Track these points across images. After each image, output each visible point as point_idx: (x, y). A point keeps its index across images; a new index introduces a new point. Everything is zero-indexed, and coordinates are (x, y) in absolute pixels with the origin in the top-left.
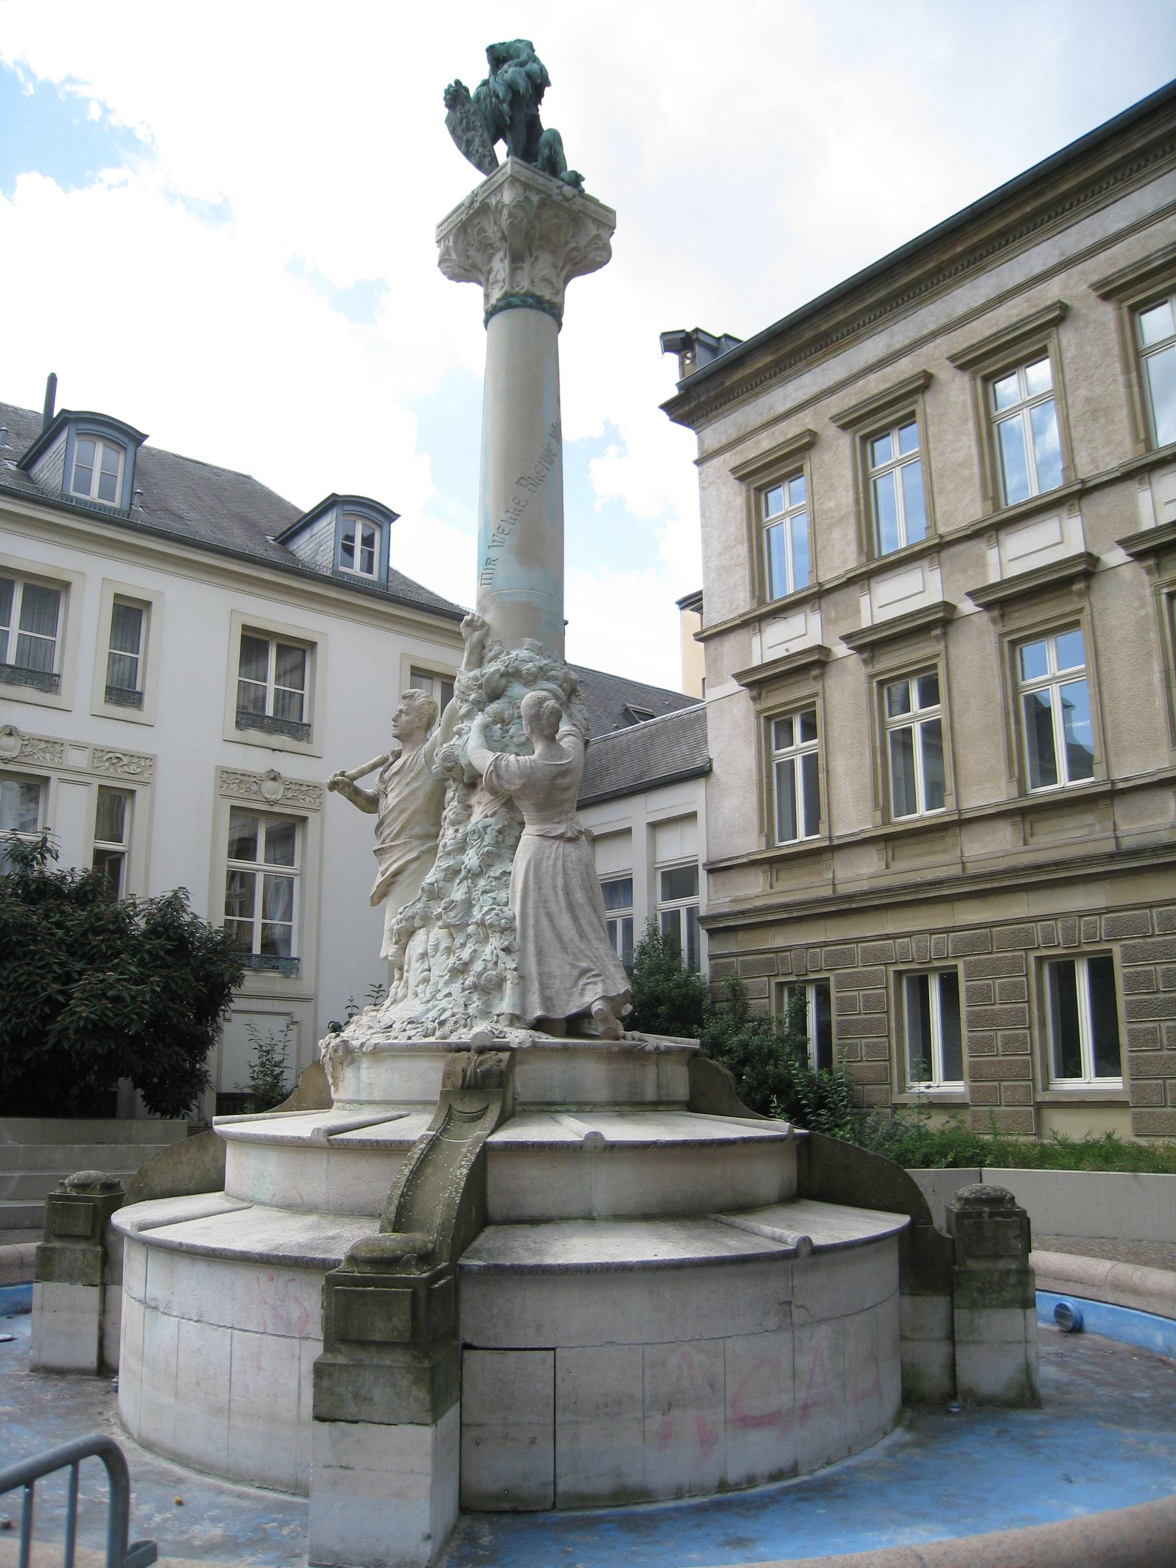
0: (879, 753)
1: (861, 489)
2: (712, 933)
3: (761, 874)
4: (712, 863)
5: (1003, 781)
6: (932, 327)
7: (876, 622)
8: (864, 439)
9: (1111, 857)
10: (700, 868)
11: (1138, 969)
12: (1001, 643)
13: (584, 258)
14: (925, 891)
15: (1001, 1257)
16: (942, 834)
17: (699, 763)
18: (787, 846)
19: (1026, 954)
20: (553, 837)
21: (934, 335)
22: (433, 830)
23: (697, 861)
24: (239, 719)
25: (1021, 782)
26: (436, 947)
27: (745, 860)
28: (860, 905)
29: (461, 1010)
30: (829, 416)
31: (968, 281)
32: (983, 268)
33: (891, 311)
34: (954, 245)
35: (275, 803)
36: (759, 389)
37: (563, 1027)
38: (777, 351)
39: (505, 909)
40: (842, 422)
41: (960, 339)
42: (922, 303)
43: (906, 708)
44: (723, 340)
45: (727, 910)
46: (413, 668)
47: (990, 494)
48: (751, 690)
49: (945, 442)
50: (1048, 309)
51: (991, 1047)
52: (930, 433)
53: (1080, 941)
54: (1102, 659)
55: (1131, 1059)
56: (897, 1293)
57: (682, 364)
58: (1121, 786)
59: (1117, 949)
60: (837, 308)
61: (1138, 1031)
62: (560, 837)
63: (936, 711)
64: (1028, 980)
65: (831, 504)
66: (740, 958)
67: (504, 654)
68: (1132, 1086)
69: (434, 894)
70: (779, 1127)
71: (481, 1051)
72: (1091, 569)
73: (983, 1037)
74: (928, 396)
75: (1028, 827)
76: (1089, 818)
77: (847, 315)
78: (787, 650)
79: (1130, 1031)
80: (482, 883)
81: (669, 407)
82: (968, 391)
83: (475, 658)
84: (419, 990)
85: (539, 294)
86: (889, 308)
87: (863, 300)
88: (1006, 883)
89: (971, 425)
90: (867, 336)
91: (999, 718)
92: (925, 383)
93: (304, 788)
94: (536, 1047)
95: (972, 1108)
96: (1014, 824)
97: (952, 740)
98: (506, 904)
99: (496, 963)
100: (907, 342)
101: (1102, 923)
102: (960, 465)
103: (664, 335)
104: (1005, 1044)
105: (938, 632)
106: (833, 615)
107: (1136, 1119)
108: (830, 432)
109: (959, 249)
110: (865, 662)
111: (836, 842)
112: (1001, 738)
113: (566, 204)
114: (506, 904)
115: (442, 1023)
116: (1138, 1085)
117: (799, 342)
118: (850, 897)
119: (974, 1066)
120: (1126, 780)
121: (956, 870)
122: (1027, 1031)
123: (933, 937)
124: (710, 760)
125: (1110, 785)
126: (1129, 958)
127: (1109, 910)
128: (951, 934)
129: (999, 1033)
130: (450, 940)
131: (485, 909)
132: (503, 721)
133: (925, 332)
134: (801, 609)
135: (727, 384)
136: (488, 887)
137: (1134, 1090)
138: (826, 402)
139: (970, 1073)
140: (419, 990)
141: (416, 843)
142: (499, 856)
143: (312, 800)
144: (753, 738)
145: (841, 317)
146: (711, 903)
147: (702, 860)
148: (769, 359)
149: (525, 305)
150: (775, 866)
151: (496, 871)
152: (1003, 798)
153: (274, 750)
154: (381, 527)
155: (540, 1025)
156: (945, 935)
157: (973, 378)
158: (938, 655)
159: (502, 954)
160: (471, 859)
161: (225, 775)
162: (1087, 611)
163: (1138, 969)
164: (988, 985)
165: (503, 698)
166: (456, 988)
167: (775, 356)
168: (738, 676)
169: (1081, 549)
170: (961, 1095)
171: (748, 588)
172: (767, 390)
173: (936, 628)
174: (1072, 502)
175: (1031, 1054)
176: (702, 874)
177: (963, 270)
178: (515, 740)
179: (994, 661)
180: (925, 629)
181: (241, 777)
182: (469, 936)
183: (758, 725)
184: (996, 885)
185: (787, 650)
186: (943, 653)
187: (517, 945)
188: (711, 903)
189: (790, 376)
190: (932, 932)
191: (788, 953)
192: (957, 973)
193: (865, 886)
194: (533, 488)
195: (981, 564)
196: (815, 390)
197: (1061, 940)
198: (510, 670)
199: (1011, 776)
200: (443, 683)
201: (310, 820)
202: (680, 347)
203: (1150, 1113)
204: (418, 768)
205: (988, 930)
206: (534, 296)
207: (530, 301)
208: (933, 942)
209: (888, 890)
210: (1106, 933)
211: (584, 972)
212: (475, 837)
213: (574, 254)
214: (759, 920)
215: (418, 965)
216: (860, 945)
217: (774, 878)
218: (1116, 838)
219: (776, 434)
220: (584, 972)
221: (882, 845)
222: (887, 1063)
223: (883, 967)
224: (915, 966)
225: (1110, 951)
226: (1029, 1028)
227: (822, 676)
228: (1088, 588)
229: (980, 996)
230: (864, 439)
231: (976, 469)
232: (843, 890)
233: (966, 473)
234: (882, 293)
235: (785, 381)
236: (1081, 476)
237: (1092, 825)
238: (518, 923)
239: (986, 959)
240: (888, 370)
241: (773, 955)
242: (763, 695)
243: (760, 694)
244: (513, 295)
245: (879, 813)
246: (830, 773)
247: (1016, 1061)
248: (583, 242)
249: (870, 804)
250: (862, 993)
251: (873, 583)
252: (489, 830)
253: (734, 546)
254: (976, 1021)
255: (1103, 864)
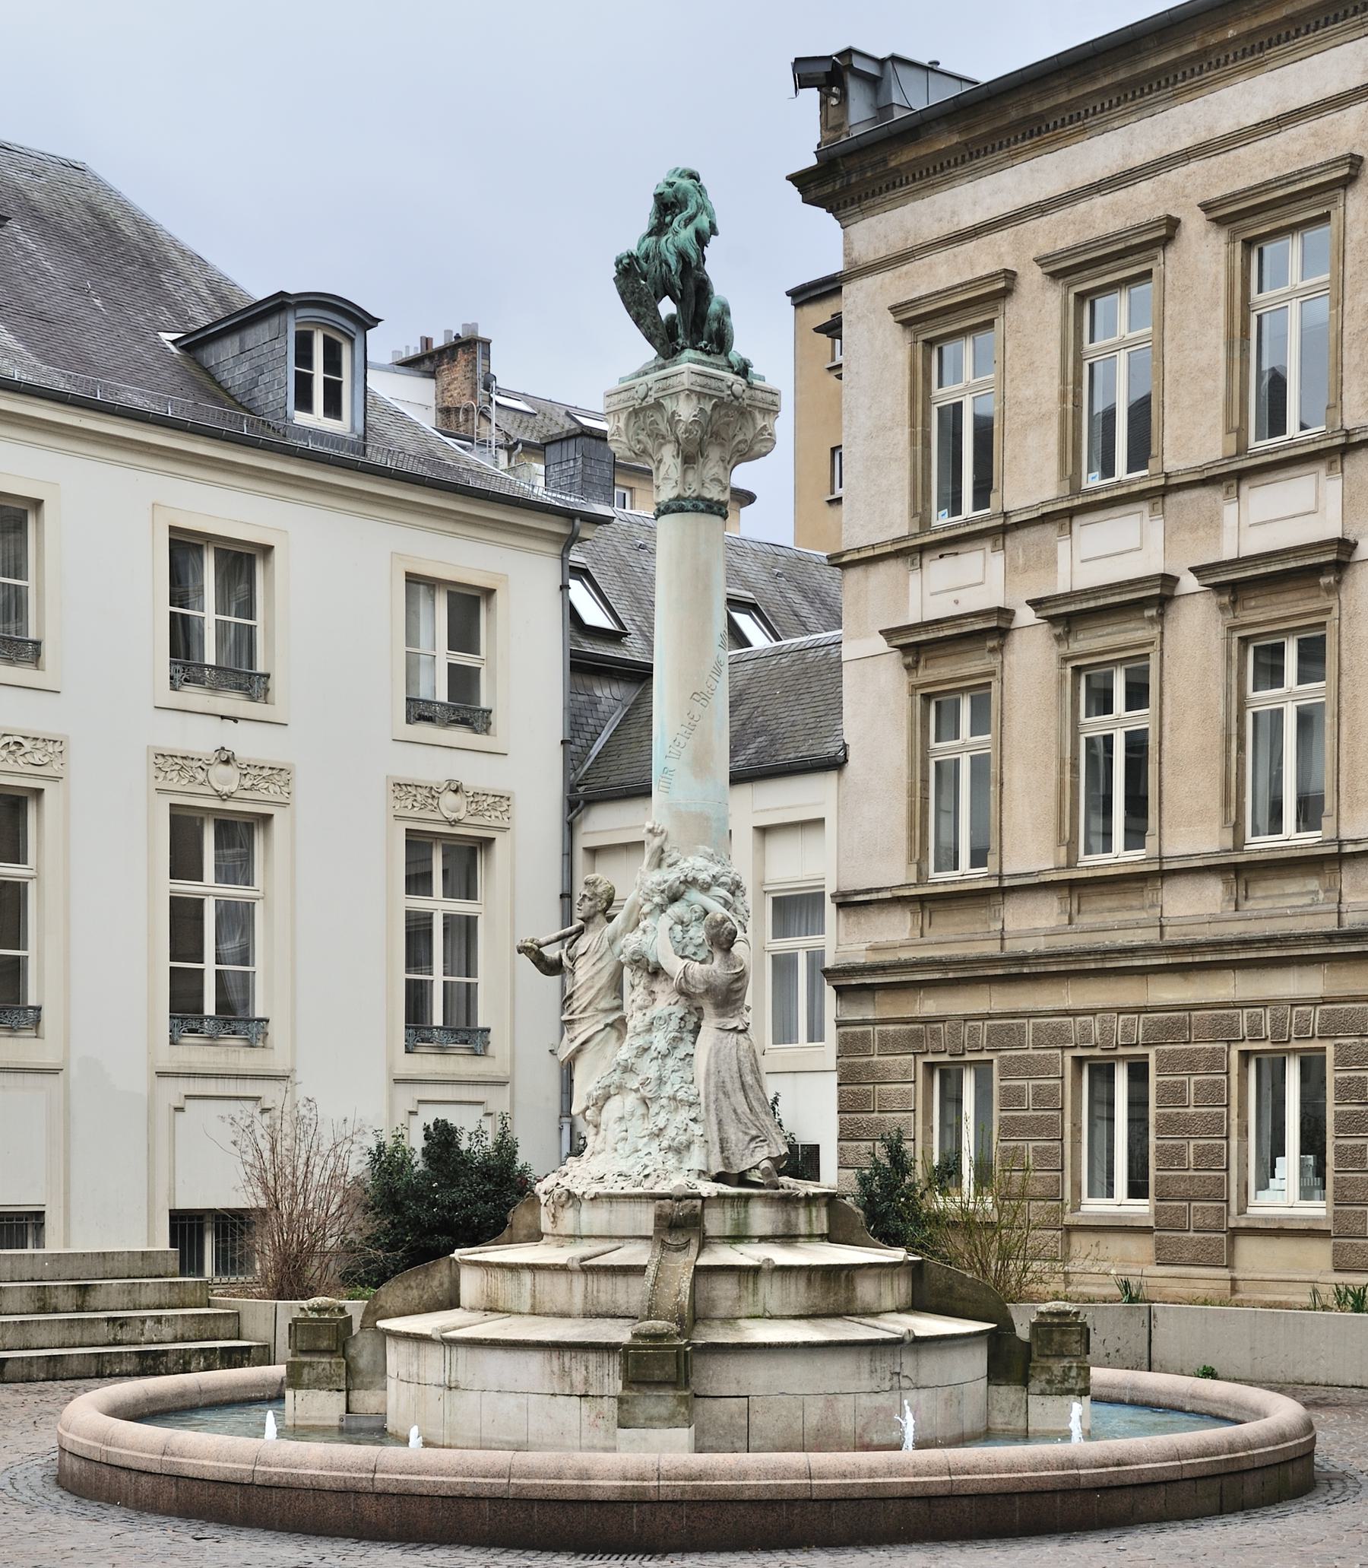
0: (1068, 768)
1: (1070, 378)
2: (840, 991)
3: (909, 915)
4: (844, 894)
5: (1217, 826)
6: (1187, 142)
7: (1074, 589)
8: (1081, 297)
9: (1330, 937)
10: (828, 899)
11: (1352, 1074)
12: (1228, 638)
13: (751, 448)
14: (1111, 959)
15: (1066, 1356)
16: (1139, 885)
17: (832, 748)
18: (941, 880)
19: (1229, 1047)
20: (729, 1030)
21: (1186, 156)
22: (616, 1003)
23: (823, 886)
24: (173, 673)
25: (1237, 828)
26: (632, 1114)
27: (887, 895)
28: (1034, 970)
29: (660, 1166)
30: (1033, 254)
31: (1242, 78)
32: (1262, 64)
33: (1133, 100)
34: (1224, 25)
35: (229, 796)
36: (938, 178)
37: (736, 1179)
38: (968, 128)
39: (691, 1086)
40: (1052, 268)
41: (1222, 171)
42: (1176, 98)
43: (1108, 709)
44: (889, 64)
45: (863, 961)
46: (407, 574)
47: (1236, 423)
48: (905, 655)
49: (1186, 332)
50: (1334, 163)
51: (1182, 1159)
52: (1168, 313)
53: (1290, 1036)
54: (1345, 679)
55: (1336, 1182)
56: (985, 1381)
57: (823, 103)
58: (1349, 848)
59: (1330, 1047)
60: (1056, 83)
61: (1346, 1148)
62: (734, 1029)
63: (1142, 719)
64: (1228, 1079)
65: (1029, 392)
66: (878, 1028)
67: (682, 861)
68: (1335, 1212)
69: (628, 1069)
70: (898, 1254)
71: (679, 1199)
72: (1344, 558)
73: (1173, 1146)
74: (1171, 254)
75: (1242, 887)
76: (1313, 884)
77: (1071, 97)
78: (957, 602)
79: (1337, 1147)
80: (670, 1062)
81: (800, 180)
82: (1222, 258)
83: (655, 860)
84: (619, 1146)
85: (708, 496)
86: (1130, 96)
87: (1094, 79)
88: (1208, 958)
89: (1221, 313)
90: (1098, 131)
91: (1217, 739)
92: (1169, 229)
93: (266, 772)
94: (721, 1197)
95: (1156, 1233)
96: (1225, 882)
97: (1160, 763)
98: (692, 1082)
99: (686, 1130)
100: (1151, 157)
101: (1316, 1015)
102: (1201, 371)
103: (798, 61)
104: (1197, 1156)
105: (1152, 612)
106: (1021, 561)
107: (1337, 1251)
108: (1032, 278)
109: (1231, 33)
110: (1058, 638)
111: (1006, 883)
112: (1218, 767)
113: (736, 403)
114: (692, 1082)
115: (646, 1176)
116: (1342, 1211)
117: (999, 124)
118: (1022, 959)
119: (1160, 1181)
120: (1356, 842)
121: (1151, 936)
122: (1224, 1142)
123: (1122, 1017)
124: (845, 746)
125: (1336, 847)
126: (1342, 1061)
127: (1325, 1001)
128: (1143, 1016)
129: (1192, 1143)
130: (644, 1107)
131: (677, 1087)
132: (682, 923)
133: (1177, 147)
134: (978, 544)
135: (892, 164)
136: (676, 1068)
137: (1337, 1217)
138: (1032, 224)
139: (1156, 1190)
140: (619, 1146)
141: (601, 1016)
142: (682, 1039)
143: (278, 789)
144: (905, 723)
145: (1063, 98)
146: (841, 949)
147: (830, 889)
148: (955, 139)
149: (696, 509)
150: (928, 905)
151: (681, 1052)
152: (1215, 848)
153: (223, 717)
154: (352, 340)
155: (719, 1178)
156: (1136, 1016)
157: (1232, 240)
158: (1152, 643)
159: (691, 1124)
160: (660, 1040)
161: (161, 760)
162: (1335, 613)
163: (1352, 1074)
164: (1183, 1083)
165: (681, 901)
166: (654, 1146)
167: (964, 138)
168: (888, 634)
169: (1333, 531)
170: (1142, 1216)
171: (907, 499)
172: (950, 181)
173: (1149, 607)
174: (1333, 458)
175: (1227, 1170)
176: (830, 907)
177: (1235, 60)
178: (694, 941)
179: (1218, 662)
180: (1137, 606)
181: (182, 762)
182: (663, 1107)
183: (913, 705)
184: (1197, 959)
185: (957, 602)
186: (1158, 642)
187: (701, 1117)
188: (841, 949)
189: (984, 168)
190: (1121, 1011)
191: (940, 1025)
192: (1147, 1063)
193: (1041, 945)
194: (705, 703)
195: (1214, 522)
196: (1019, 201)
197: (1269, 1033)
198: (690, 879)
199: (1226, 820)
200: (449, 593)
201: (275, 819)
202: (824, 82)
203: (1352, 1245)
204: (602, 950)
205: (1187, 1013)
206: (704, 499)
207: (702, 506)
208: (1120, 1023)
209: (1068, 954)
210: (1319, 1028)
211: (753, 1139)
212: (662, 1022)
213: (742, 446)
214: (904, 978)
215: (616, 1126)
216: (1032, 1021)
217: (926, 921)
218: (1339, 913)
219: (960, 260)
220: (753, 1139)
221: (1065, 893)
222: (1060, 1174)
223: (1059, 1052)
224: (1097, 1052)
225: (1324, 1049)
226: (1227, 1138)
227: (999, 649)
228: (1339, 582)
229: (1173, 1095)
230: (1081, 297)
231: (1222, 383)
232: (1014, 947)
233: (1209, 385)
234: (1122, 75)
235: (977, 173)
236: (1349, 425)
237: (1316, 893)
238: (702, 1099)
239: (1183, 1050)
240: (1121, 195)
241: (921, 1026)
242: (922, 663)
243: (917, 662)
244: (684, 499)
245: (1064, 849)
246: (1005, 786)
247: (1210, 1177)
248: (750, 436)
249: (1052, 836)
250: (1031, 1083)
251: (1077, 522)
252: (673, 1017)
253: (891, 429)
254: (1167, 1125)
255: (1318, 945)
